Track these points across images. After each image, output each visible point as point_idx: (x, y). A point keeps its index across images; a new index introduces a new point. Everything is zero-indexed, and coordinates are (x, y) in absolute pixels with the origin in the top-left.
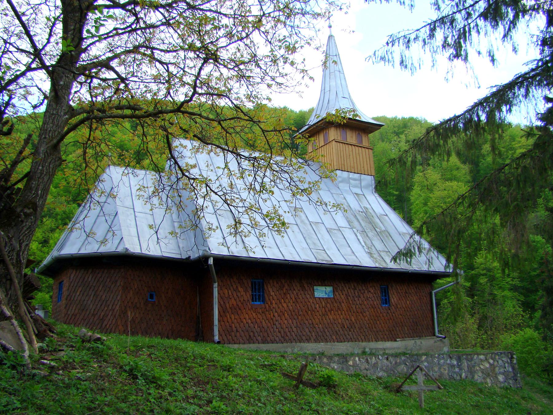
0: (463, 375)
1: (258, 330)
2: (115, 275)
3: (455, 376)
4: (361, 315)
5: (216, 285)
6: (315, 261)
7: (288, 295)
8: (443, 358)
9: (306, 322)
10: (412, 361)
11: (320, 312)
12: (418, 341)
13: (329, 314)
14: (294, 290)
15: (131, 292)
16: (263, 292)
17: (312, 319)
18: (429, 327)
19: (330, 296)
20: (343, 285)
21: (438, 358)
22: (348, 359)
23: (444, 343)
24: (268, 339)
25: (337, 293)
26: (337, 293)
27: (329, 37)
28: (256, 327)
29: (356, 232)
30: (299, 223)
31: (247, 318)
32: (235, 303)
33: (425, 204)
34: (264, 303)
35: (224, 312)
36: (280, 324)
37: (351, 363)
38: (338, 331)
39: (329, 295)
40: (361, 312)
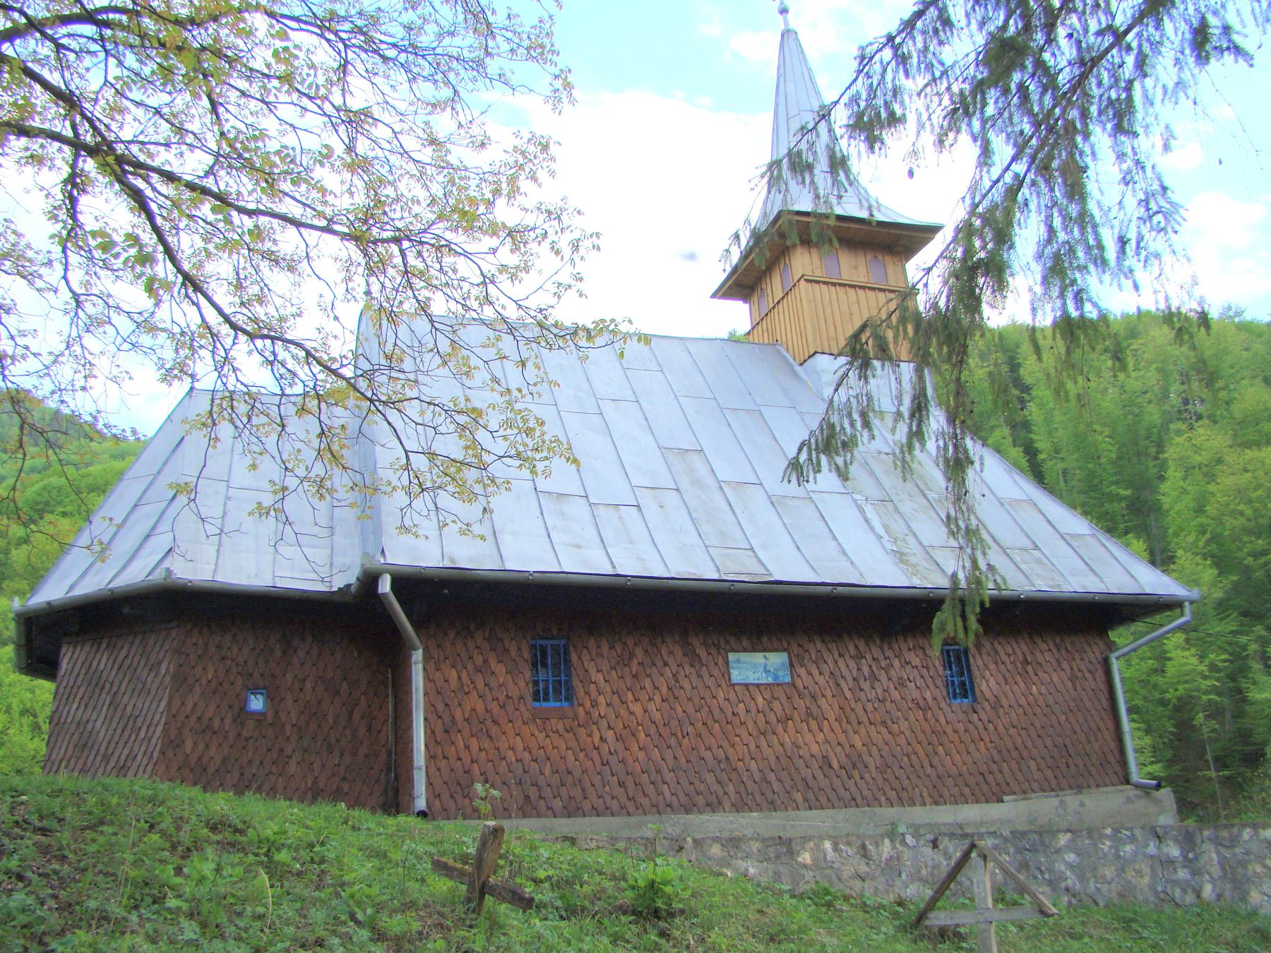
0: (1208, 891)
1: (555, 780)
2: (157, 649)
3: (1178, 893)
4: (883, 730)
5: (418, 656)
6: (715, 576)
7: (647, 681)
8: (1132, 839)
9: (707, 755)
10: (1019, 851)
11: (750, 725)
12: (1072, 801)
13: (780, 730)
14: (666, 664)
15: (197, 690)
16: (569, 675)
17: (726, 745)
18: (1111, 758)
19: (781, 680)
20: (819, 644)
21: (1113, 837)
22: (796, 847)
23: (1158, 802)
24: (586, 805)
25: (802, 671)
26: (802, 671)
27: (783, 36)
28: (547, 771)
29: (863, 503)
30: (684, 483)
31: (520, 746)
32: (480, 707)
33: (1200, 510)
34: (572, 704)
35: (446, 731)
36: (623, 761)
37: (806, 857)
38: (810, 779)
39: (776, 677)
40: (884, 723)
